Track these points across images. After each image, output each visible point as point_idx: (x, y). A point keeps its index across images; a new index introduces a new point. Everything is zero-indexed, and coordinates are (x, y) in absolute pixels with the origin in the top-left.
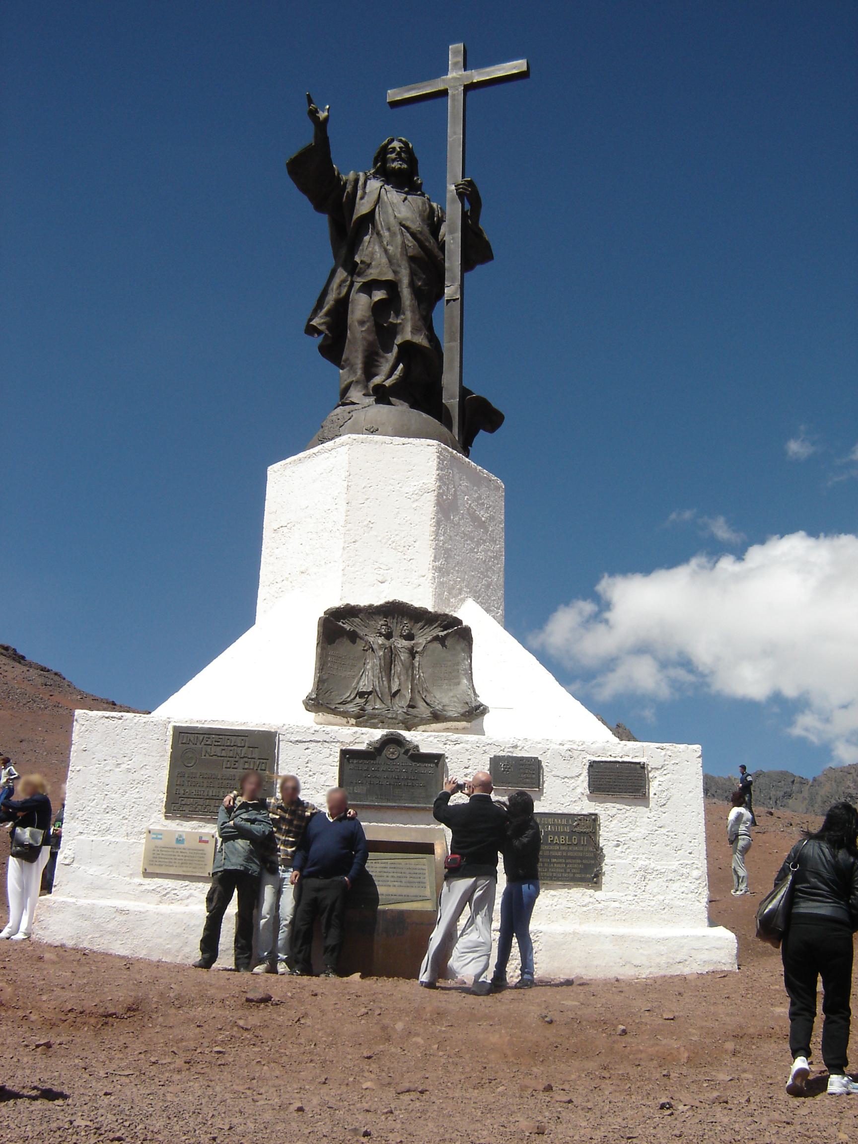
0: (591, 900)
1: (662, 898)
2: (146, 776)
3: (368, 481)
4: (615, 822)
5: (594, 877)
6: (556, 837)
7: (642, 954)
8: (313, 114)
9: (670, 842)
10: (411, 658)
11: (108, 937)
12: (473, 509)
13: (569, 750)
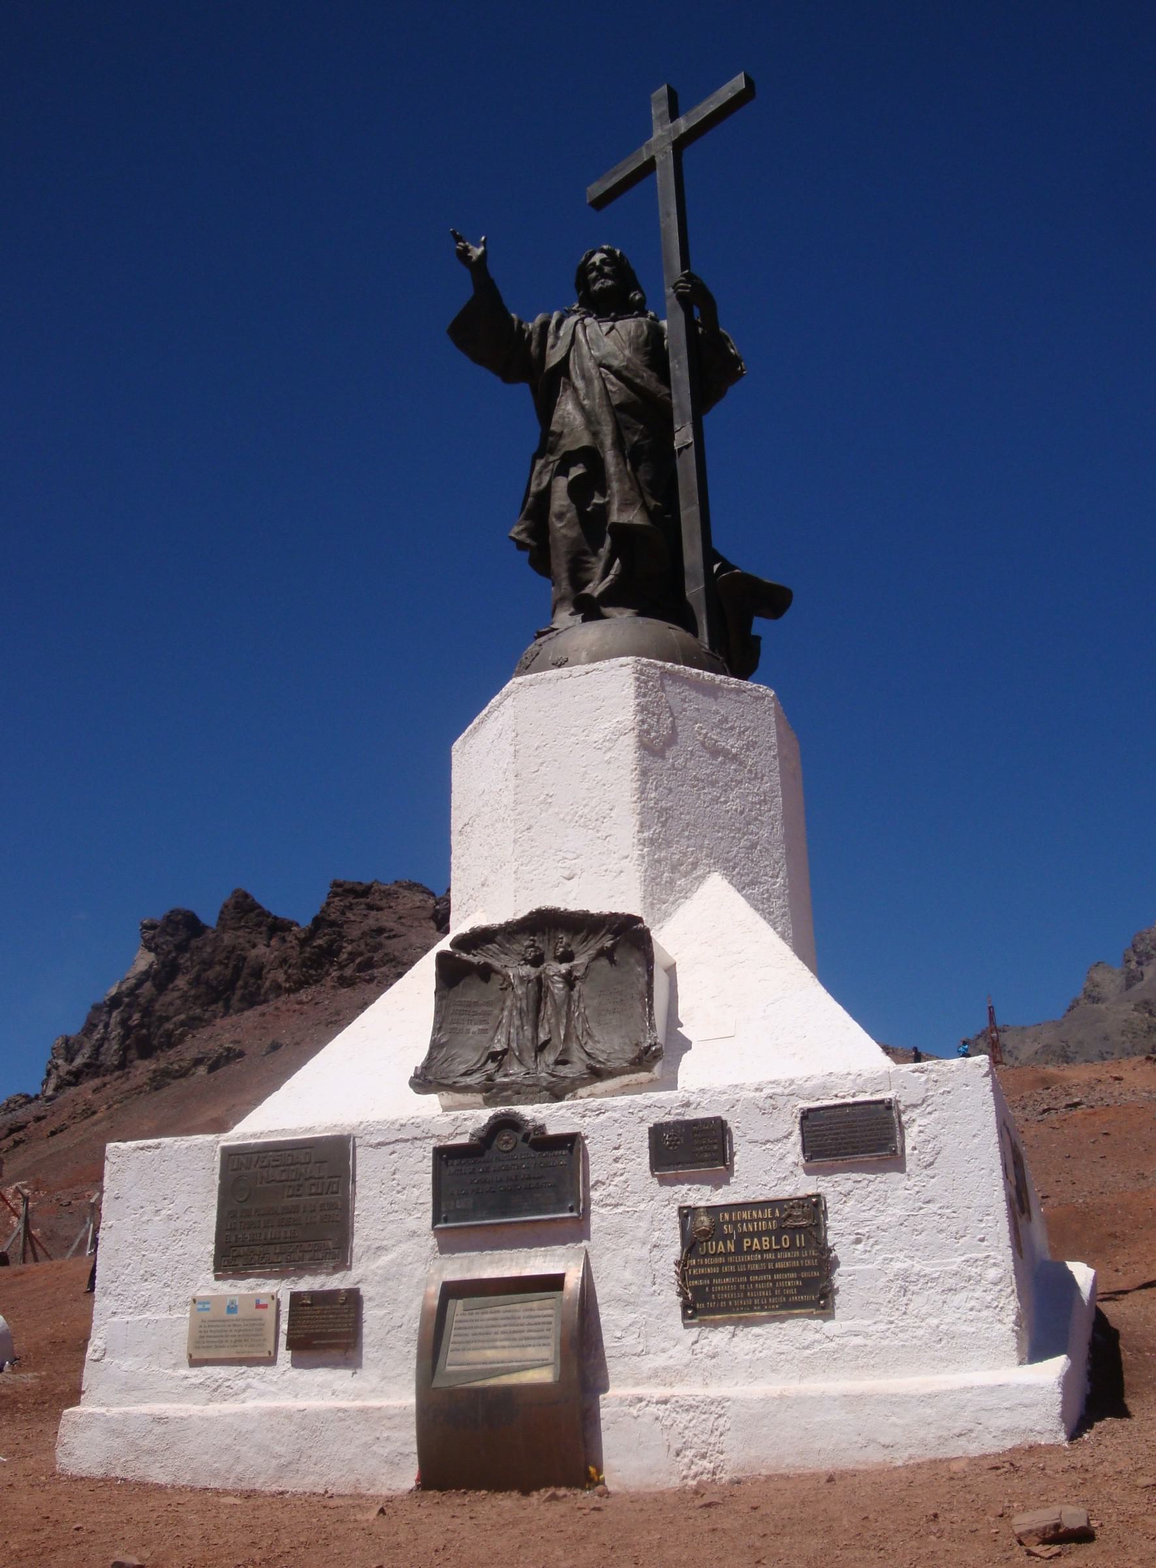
0: (818, 1336)
1: (936, 1321)
2: (191, 1223)
3: (543, 738)
4: (851, 1203)
5: (820, 1299)
6: (756, 1240)
7: (895, 1425)
8: (463, 255)
9: (945, 1225)
10: (567, 989)
11: (144, 1460)
12: (712, 739)
13: (771, 1097)
